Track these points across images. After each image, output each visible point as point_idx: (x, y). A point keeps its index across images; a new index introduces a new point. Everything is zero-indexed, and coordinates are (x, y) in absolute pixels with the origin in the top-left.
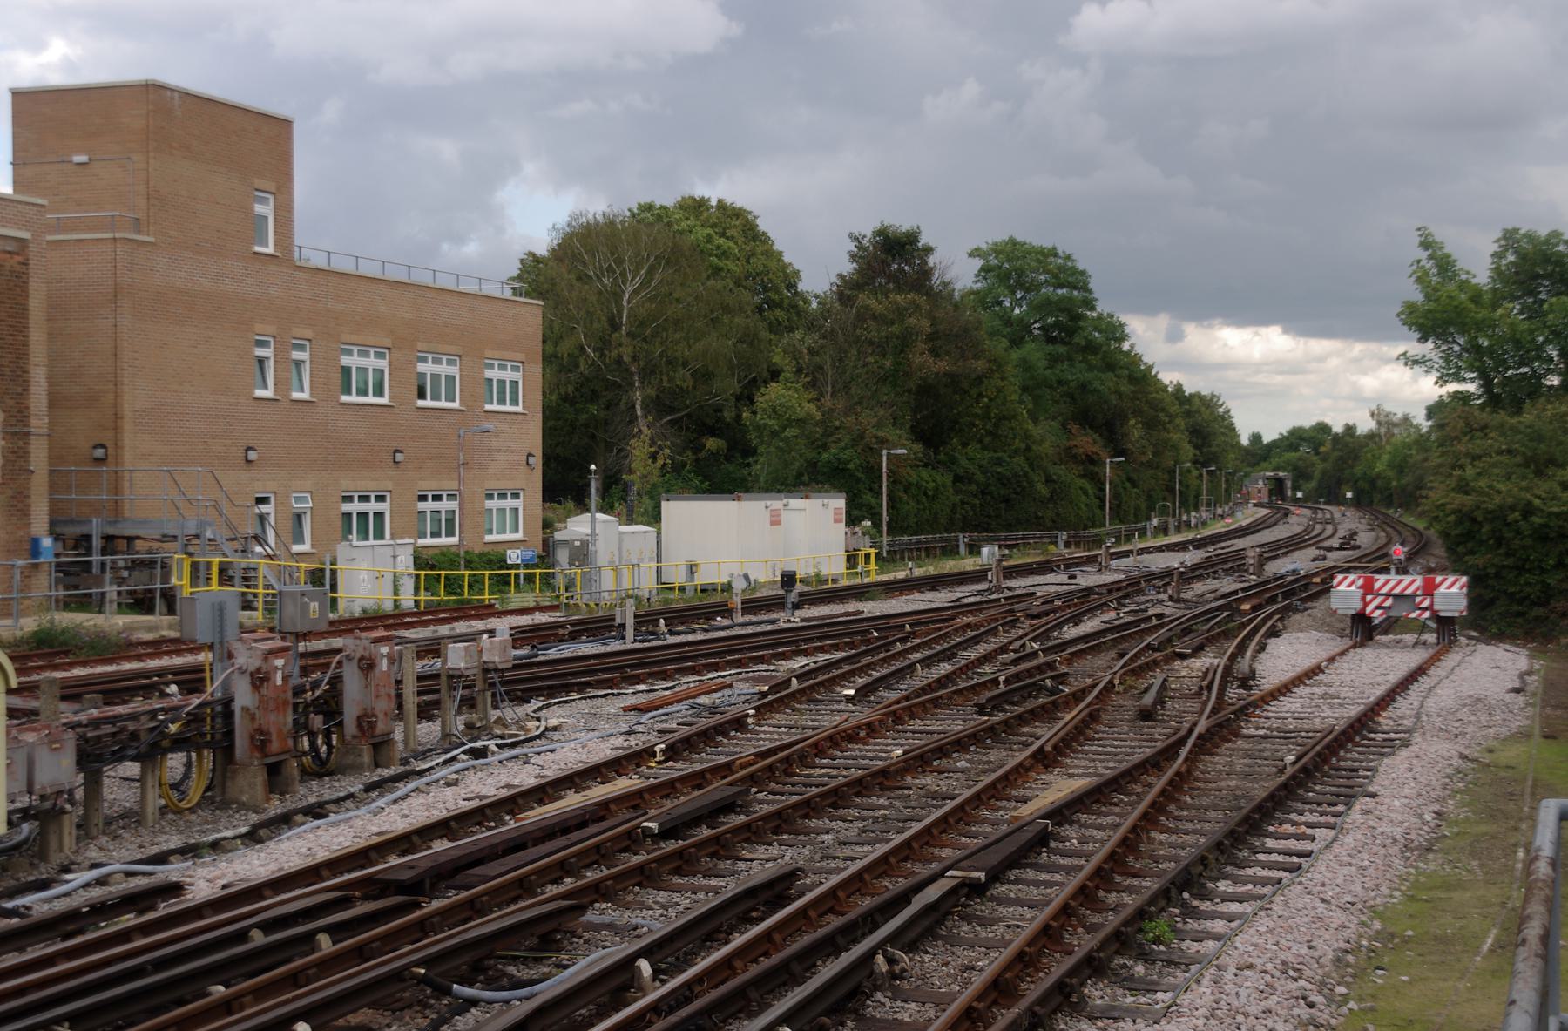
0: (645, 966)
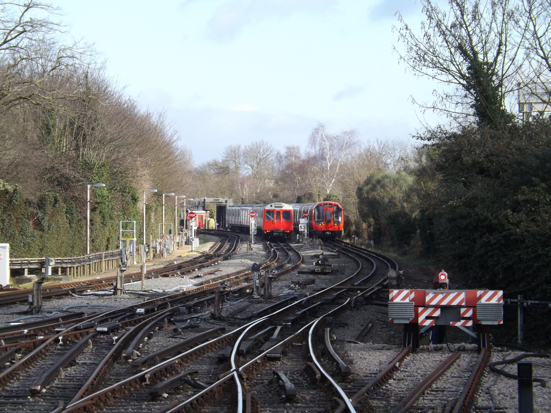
0: (156, 309)
